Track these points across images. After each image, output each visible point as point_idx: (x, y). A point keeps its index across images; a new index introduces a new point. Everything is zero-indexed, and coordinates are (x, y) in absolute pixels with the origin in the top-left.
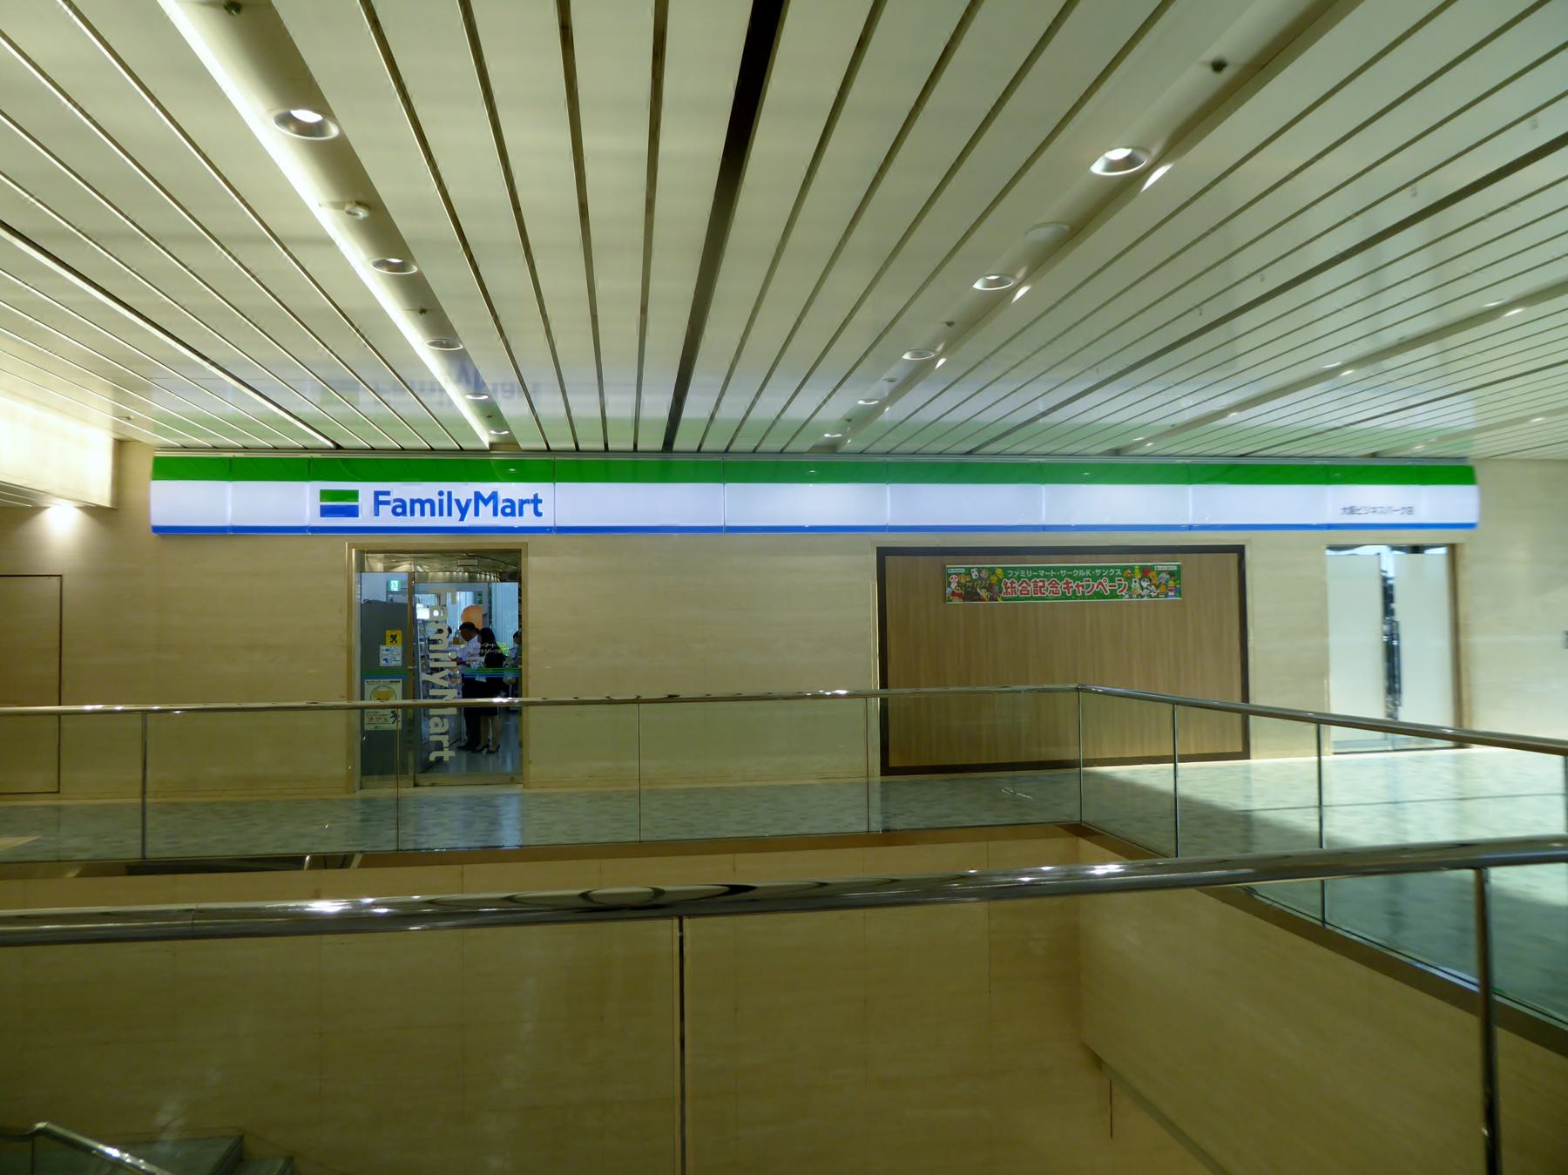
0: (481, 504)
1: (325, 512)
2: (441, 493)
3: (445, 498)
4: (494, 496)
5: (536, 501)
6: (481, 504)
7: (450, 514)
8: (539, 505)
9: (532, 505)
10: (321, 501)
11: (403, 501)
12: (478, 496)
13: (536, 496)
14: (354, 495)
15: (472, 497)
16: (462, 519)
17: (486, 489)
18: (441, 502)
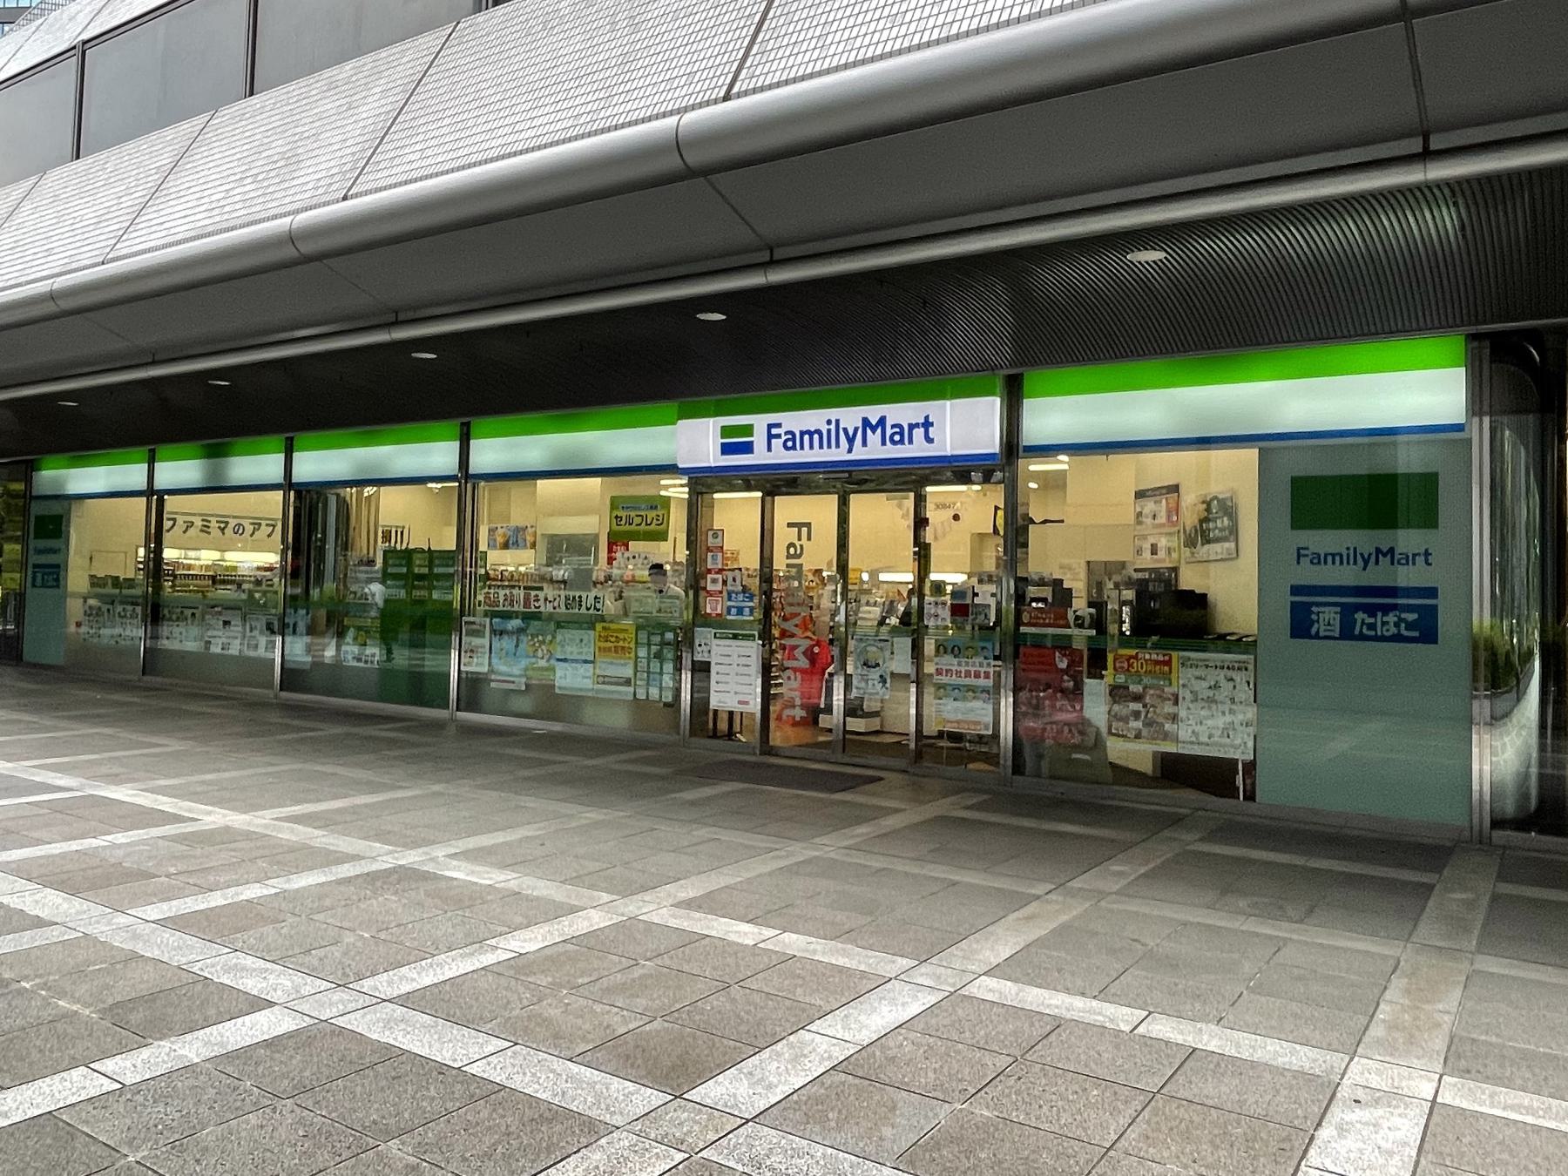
0: (869, 431)
1: (727, 449)
2: (829, 422)
3: (833, 427)
4: (882, 421)
5: (927, 424)
6: (869, 431)
7: (838, 446)
8: (1430, 557)
12: (866, 422)
16: (850, 451)
17: (874, 413)
18: (829, 431)
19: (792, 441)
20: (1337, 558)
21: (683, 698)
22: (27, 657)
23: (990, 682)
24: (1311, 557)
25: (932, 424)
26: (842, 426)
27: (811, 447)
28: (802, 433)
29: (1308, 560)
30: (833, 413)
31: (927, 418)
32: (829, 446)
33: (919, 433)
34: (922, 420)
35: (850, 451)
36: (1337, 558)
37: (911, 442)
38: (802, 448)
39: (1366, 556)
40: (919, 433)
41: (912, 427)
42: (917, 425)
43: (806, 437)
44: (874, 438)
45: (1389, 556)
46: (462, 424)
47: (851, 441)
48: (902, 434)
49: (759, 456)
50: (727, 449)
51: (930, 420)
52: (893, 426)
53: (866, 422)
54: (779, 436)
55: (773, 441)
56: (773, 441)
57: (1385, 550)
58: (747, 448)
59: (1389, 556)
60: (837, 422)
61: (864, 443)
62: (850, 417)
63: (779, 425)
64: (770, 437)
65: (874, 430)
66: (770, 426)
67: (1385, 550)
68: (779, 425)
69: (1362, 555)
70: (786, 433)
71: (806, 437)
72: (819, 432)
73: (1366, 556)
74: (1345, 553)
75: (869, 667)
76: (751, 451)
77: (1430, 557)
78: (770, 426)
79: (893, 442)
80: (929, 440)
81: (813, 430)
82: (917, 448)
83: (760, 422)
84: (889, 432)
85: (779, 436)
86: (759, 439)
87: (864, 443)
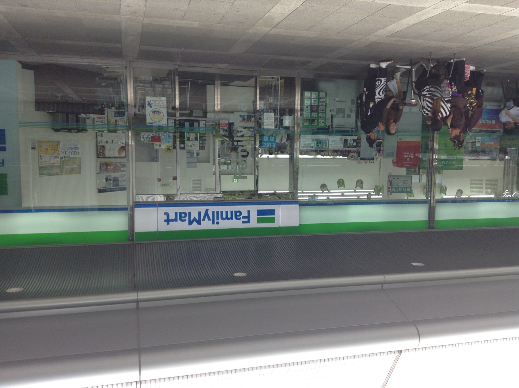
0: (197, 218)
1: (272, 212)
2: (218, 223)
3: (216, 221)
4: (190, 223)
5: (168, 221)
6: (197, 218)
7: (213, 213)
8: (166, 219)
9: (170, 218)
10: (274, 217)
11: (236, 218)
12: (199, 223)
13: (168, 224)
14: (259, 221)
15: (202, 222)
16: (207, 210)
17: (195, 226)
18: (218, 219)
19: (237, 215)
20: (224, 216)
21: (132, 90)
22: (406, 90)
23: (320, 121)
24: (241, 217)
25: (165, 221)
26: (211, 222)
27: (227, 212)
28: (231, 218)
29: (243, 215)
30: (215, 227)
31: (168, 224)
32: (218, 212)
33: (172, 217)
34: (171, 223)
35: (207, 210)
36: (224, 216)
37: (176, 213)
38: (232, 212)
39: (206, 218)
40: (172, 217)
41: (175, 220)
42: (173, 220)
43: (229, 216)
44: (195, 215)
45: (192, 218)
46: (433, 228)
47: (206, 214)
48: (181, 217)
49: (254, 209)
50: (272, 212)
51: (166, 223)
52: (185, 220)
53: (199, 223)
54: (244, 217)
55: (247, 215)
56: (247, 215)
57: (195, 223)
58: (260, 212)
59: (192, 218)
60: (213, 223)
61: (199, 213)
62: (206, 225)
63: (243, 222)
64: (248, 217)
65: (195, 218)
66: (249, 222)
67: (195, 223)
68: (243, 222)
69: (209, 219)
70: (240, 219)
71: (229, 216)
72: (223, 219)
73: (206, 218)
74: (220, 220)
75: (158, 111)
76: (258, 211)
77: (166, 219)
78: (249, 222)
79: (185, 213)
80: (167, 214)
81: (226, 220)
82: (172, 211)
83: (254, 224)
84: (187, 218)
85: (244, 217)
86: (254, 216)
87: (199, 213)
